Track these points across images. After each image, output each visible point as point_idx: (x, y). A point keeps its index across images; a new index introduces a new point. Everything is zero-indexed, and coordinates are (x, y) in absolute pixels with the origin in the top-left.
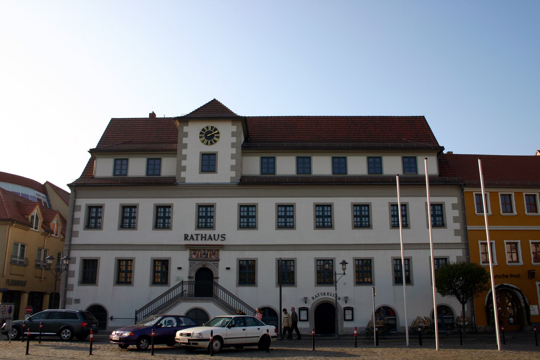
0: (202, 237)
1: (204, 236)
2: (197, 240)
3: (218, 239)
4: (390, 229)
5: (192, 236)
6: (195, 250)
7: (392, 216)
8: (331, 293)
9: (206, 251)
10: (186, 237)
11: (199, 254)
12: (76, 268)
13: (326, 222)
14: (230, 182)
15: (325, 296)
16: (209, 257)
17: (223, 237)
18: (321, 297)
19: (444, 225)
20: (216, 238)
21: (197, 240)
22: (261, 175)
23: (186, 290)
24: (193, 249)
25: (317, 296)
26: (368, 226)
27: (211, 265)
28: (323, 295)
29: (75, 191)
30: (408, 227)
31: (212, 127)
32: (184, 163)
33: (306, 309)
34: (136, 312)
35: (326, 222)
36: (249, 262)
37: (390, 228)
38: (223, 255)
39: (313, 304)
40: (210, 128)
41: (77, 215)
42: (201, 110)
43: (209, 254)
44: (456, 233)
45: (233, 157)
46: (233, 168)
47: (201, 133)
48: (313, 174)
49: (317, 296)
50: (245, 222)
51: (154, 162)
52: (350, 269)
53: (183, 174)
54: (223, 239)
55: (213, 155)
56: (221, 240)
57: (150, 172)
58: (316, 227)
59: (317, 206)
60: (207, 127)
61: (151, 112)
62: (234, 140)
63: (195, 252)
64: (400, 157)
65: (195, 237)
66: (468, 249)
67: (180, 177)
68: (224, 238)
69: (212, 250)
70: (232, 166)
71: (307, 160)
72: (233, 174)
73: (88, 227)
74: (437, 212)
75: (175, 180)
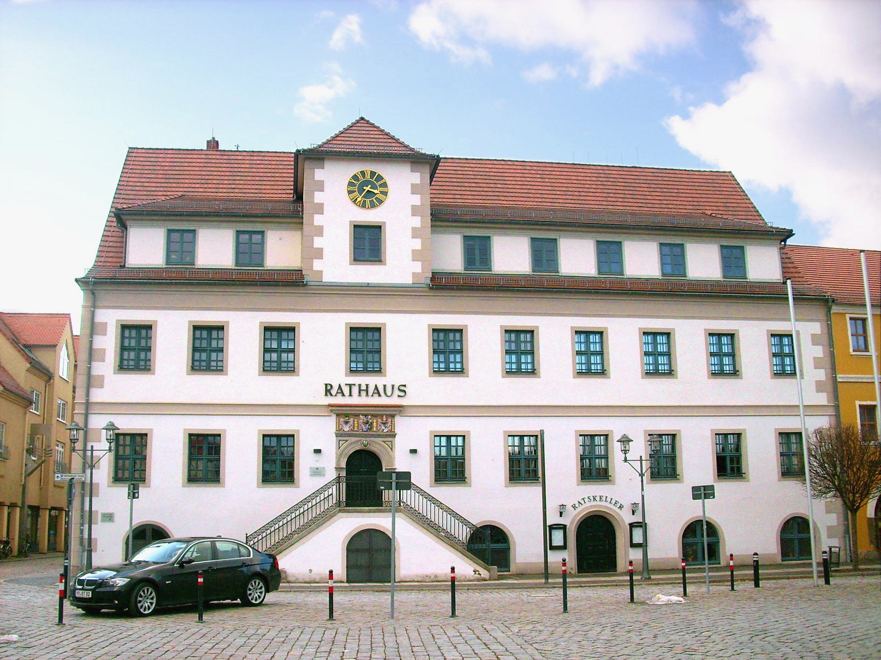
0: (360, 391)
1: (364, 387)
2: (350, 395)
3: (392, 393)
4: (709, 378)
5: (340, 387)
6: (347, 415)
7: (506, 353)
8: (606, 497)
9: (369, 417)
10: (328, 391)
11: (356, 423)
12: (102, 447)
13: (143, 360)
14: (411, 283)
15: (595, 503)
16: (375, 429)
17: (402, 389)
18: (588, 504)
19: (737, 373)
20: (389, 393)
21: (350, 395)
22: (236, 266)
23: (332, 494)
24: (342, 413)
25: (582, 502)
26: (459, 370)
27: (379, 444)
28: (592, 500)
29: (93, 294)
30: (536, 374)
31: (373, 174)
32: (318, 242)
33: (564, 528)
34: (247, 537)
35: (143, 360)
36: (209, 438)
37: (346, 374)
38: (401, 425)
39: (576, 516)
40: (369, 175)
41: (99, 342)
42: (339, 139)
43: (375, 424)
44: (819, 387)
45: (416, 233)
46: (416, 255)
47: (350, 184)
48: (628, 273)
49: (582, 502)
50: (204, 361)
51: (251, 239)
52: (640, 449)
53: (317, 265)
54: (402, 394)
55: (377, 229)
56: (399, 396)
57: (668, 269)
58: (351, 371)
59: (353, 329)
60: (363, 173)
61: (210, 139)
62: (416, 200)
63: (347, 418)
64: (232, 231)
65: (346, 390)
66: (839, 415)
67: (312, 269)
68: (405, 391)
69: (382, 416)
70: (414, 252)
71: (256, 238)
72: (417, 267)
73: (122, 367)
74: (592, 346)
75: (302, 276)
